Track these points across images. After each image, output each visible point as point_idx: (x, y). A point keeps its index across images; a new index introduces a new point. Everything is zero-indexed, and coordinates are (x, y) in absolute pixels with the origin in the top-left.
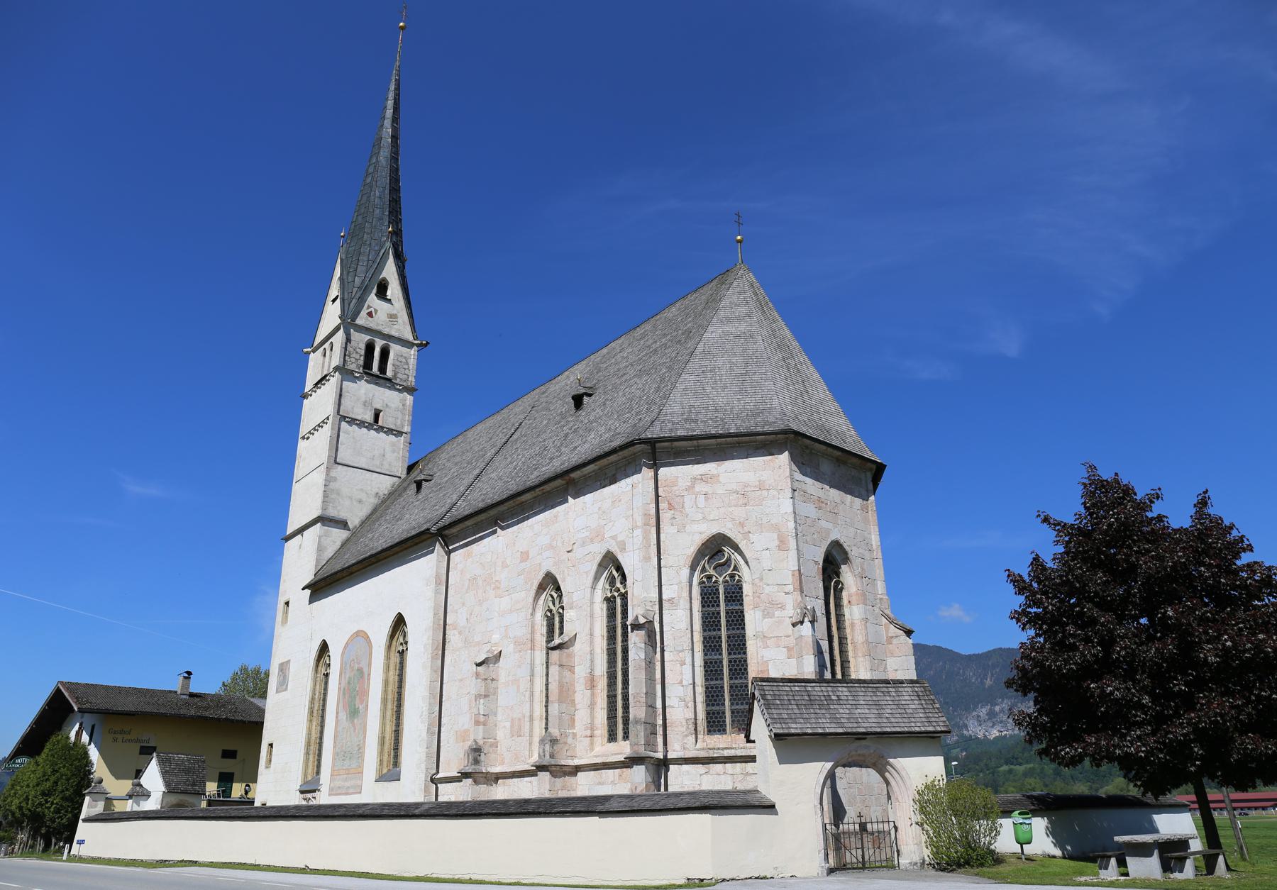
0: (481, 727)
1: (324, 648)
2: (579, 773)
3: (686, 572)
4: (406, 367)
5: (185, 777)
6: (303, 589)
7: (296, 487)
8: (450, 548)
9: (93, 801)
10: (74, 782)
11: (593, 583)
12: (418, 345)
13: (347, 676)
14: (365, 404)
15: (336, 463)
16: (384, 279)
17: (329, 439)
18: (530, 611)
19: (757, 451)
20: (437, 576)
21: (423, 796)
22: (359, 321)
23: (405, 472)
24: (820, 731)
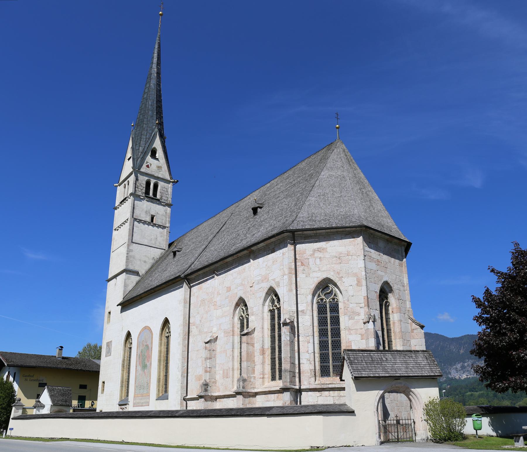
1: (129, 335)
2: (257, 396)
4: (167, 193)
5: (62, 398)
7: (112, 255)
8: (191, 285)
9: (17, 409)
10: (7, 400)
12: (173, 182)
14: (146, 212)
16: (155, 148)
18: (232, 316)
19: (347, 236)
24: (377, 375)
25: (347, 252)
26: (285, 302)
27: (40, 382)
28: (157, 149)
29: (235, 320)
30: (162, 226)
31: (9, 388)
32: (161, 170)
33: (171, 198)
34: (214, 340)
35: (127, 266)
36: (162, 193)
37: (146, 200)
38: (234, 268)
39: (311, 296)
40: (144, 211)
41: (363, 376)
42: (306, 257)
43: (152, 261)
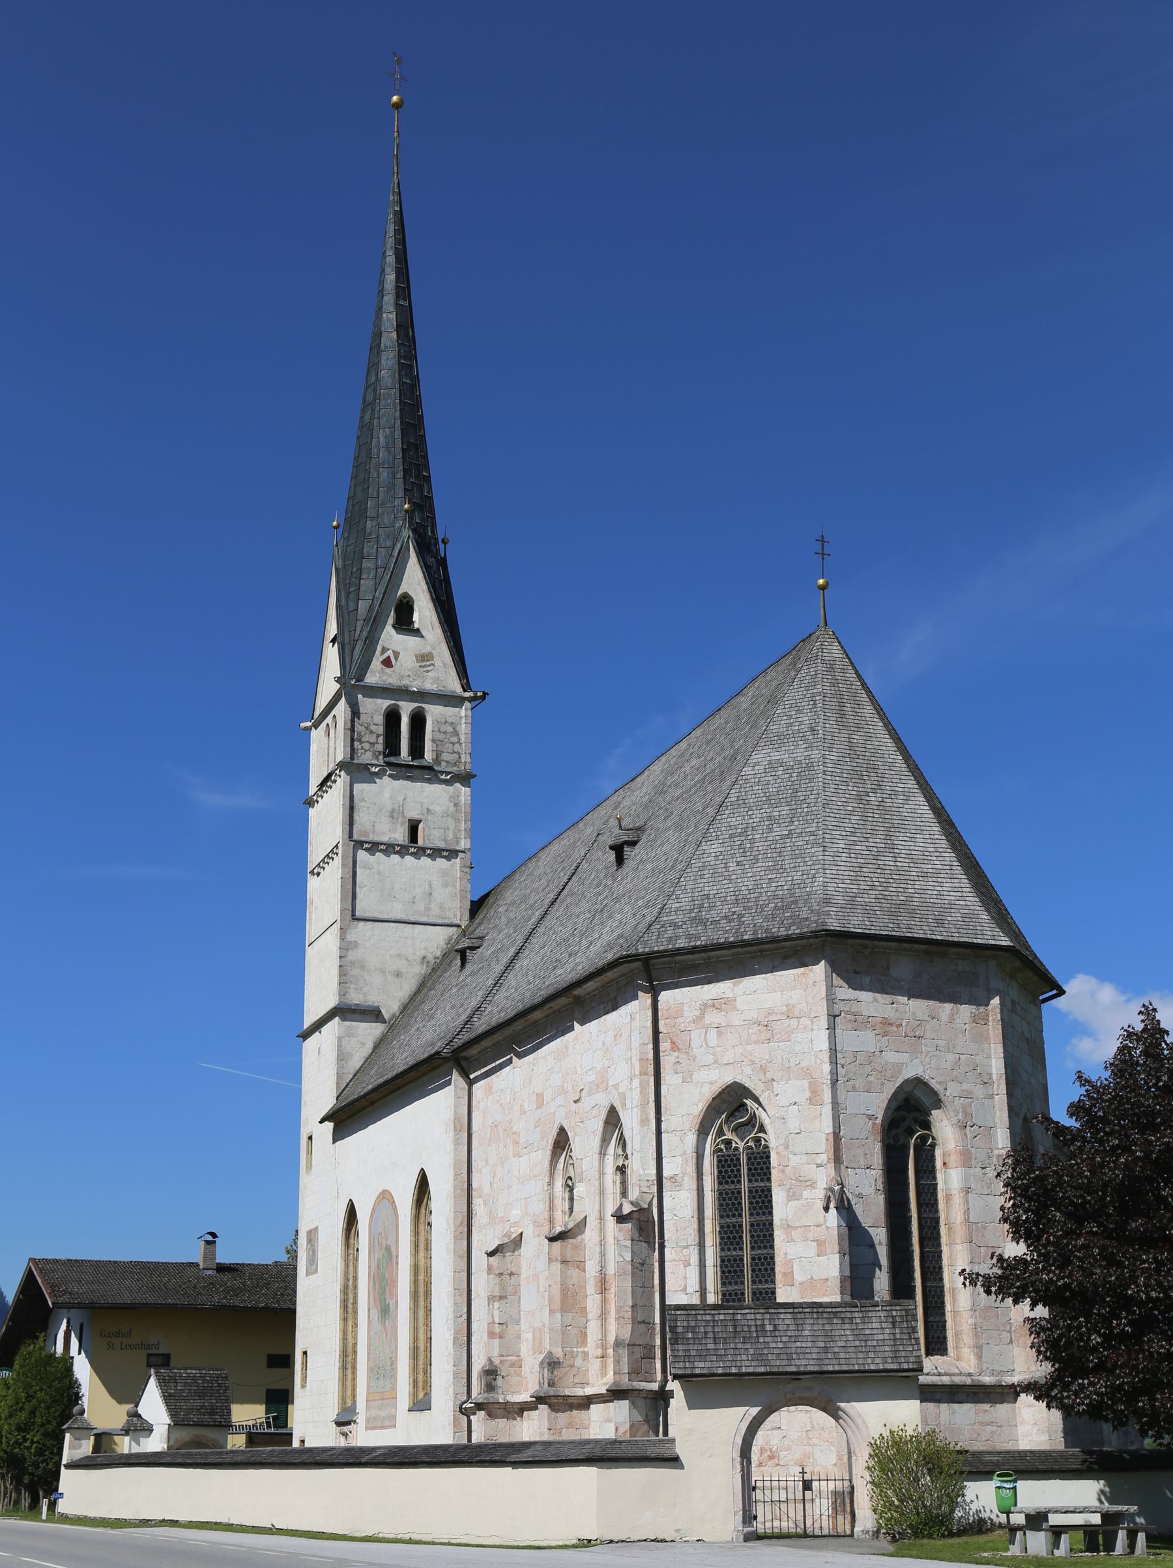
0: (497, 1341)
2: (591, 1406)
3: (691, 1139)
4: (455, 739)
5: (198, 1403)
6: (321, 1122)
7: (310, 952)
8: (472, 1076)
9: (75, 1439)
10: (56, 1411)
11: (601, 1147)
12: (470, 700)
13: (376, 1257)
14: (392, 815)
15: (354, 918)
16: (406, 596)
17: (340, 881)
18: (547, 1179)
19: (786, 961)
20: (456, 1119)
21: (452, 1432)
22: (371, 679)
23: (467, 915)
24: (734, 1370)
26: (635, 1153)
27: (150, 1352)
28: (414, 599)
29: (555, 1190)
30: (444, 850)
31: (59, 1375)
32: (429, 666)
33: (470, 754)
34: (513, 1245)
36: (439, 743)
37: (390, 776)
38: (549, 1040)
39: (695, 1136)
40: (384, 811)
41: (697, 1372)
42: (682, 1025)
43: (420, 970)
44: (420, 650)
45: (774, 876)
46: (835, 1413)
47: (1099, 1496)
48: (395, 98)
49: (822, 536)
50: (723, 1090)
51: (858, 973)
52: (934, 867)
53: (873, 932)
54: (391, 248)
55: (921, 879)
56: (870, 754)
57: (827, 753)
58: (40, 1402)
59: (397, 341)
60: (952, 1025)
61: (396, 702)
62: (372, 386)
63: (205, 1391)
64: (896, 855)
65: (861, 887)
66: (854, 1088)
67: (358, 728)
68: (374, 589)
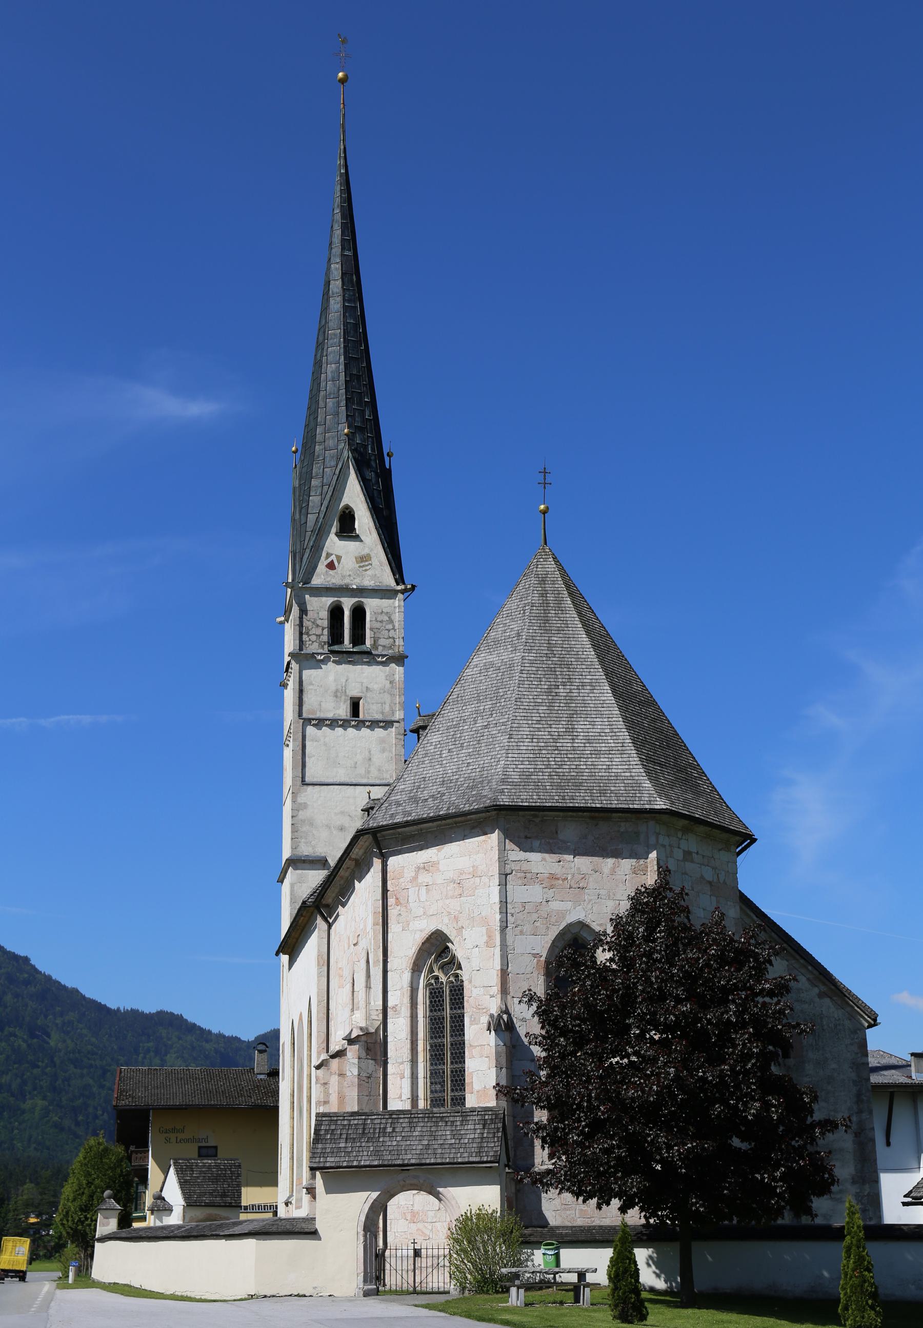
3: (407, 976)
4: (390, 627)
5: (211, 1187)
9: (104, 1218)
12: (403, 592)
16: (347, 507)
19: (473, 831)
24: (355, 1163)
25: (471, 869)
27: (201, 1144)
28: (355, 509)
30: (381, 722)
32: (367, 565)
35: (296, 848)
37: (334, 662)
41: (328, 1165)
44: (359, 553)
45: (471, 761)
46: (437, 1195)
47: (648, 1260)
48: (341, 75)
49: (545, 468)
50: (430, 936)
51: (530, 838)
52: (607, 745)
53: (538, 804)
54: (338, 206)
55: (593, 756)
56: (566, 653)
57: (527, 654)
58: (96, 1188)
59: (342, 287)
60: (614, 877)
61: (338, 599)
62: (323, 329)
63: (218, 1178)
64: (575, 737)
65: (538, 767)
66: (522, 933)
67: (306, 623)
68: (320, 504)
